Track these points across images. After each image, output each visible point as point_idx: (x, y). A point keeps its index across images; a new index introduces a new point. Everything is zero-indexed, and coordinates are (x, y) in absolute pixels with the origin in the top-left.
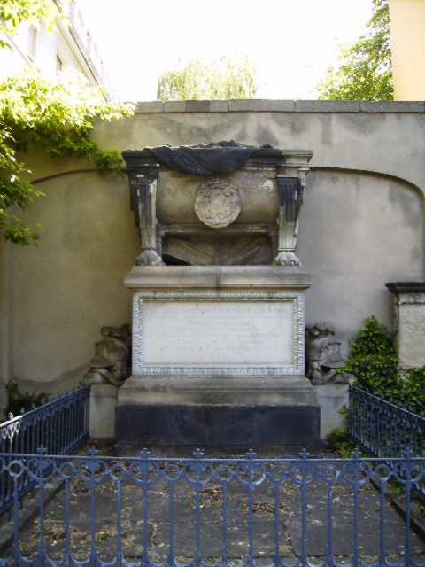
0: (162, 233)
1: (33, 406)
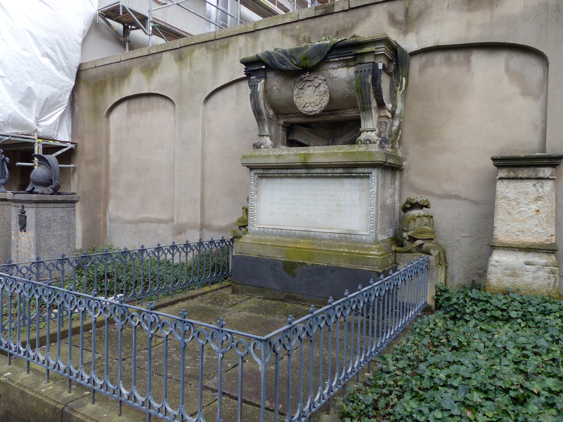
0: (282, 122)
1: (371, 282)
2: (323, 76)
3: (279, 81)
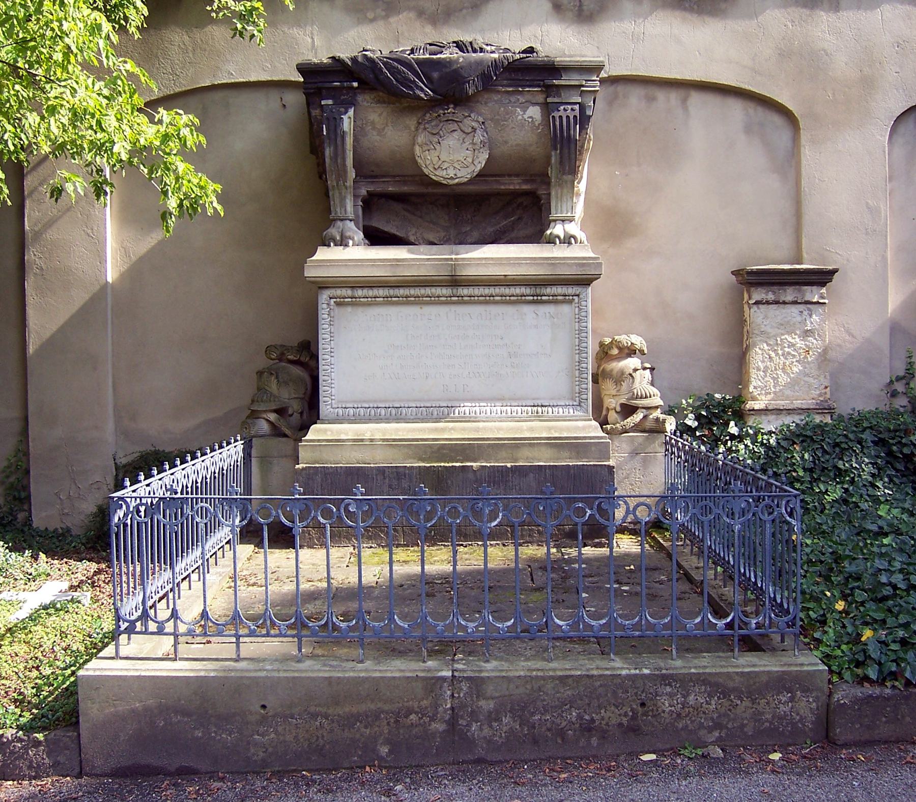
0: (363, 192)
2: (480, 114)
3: (385, 114)
